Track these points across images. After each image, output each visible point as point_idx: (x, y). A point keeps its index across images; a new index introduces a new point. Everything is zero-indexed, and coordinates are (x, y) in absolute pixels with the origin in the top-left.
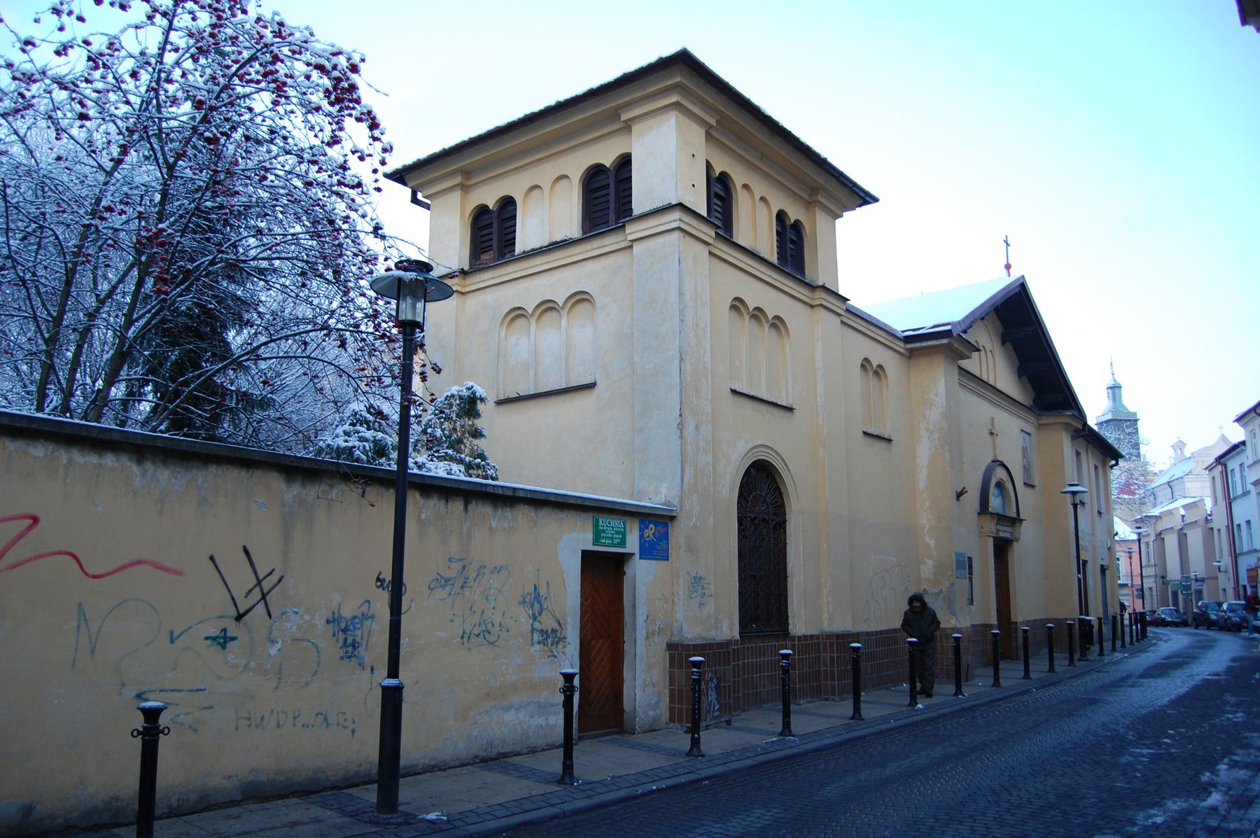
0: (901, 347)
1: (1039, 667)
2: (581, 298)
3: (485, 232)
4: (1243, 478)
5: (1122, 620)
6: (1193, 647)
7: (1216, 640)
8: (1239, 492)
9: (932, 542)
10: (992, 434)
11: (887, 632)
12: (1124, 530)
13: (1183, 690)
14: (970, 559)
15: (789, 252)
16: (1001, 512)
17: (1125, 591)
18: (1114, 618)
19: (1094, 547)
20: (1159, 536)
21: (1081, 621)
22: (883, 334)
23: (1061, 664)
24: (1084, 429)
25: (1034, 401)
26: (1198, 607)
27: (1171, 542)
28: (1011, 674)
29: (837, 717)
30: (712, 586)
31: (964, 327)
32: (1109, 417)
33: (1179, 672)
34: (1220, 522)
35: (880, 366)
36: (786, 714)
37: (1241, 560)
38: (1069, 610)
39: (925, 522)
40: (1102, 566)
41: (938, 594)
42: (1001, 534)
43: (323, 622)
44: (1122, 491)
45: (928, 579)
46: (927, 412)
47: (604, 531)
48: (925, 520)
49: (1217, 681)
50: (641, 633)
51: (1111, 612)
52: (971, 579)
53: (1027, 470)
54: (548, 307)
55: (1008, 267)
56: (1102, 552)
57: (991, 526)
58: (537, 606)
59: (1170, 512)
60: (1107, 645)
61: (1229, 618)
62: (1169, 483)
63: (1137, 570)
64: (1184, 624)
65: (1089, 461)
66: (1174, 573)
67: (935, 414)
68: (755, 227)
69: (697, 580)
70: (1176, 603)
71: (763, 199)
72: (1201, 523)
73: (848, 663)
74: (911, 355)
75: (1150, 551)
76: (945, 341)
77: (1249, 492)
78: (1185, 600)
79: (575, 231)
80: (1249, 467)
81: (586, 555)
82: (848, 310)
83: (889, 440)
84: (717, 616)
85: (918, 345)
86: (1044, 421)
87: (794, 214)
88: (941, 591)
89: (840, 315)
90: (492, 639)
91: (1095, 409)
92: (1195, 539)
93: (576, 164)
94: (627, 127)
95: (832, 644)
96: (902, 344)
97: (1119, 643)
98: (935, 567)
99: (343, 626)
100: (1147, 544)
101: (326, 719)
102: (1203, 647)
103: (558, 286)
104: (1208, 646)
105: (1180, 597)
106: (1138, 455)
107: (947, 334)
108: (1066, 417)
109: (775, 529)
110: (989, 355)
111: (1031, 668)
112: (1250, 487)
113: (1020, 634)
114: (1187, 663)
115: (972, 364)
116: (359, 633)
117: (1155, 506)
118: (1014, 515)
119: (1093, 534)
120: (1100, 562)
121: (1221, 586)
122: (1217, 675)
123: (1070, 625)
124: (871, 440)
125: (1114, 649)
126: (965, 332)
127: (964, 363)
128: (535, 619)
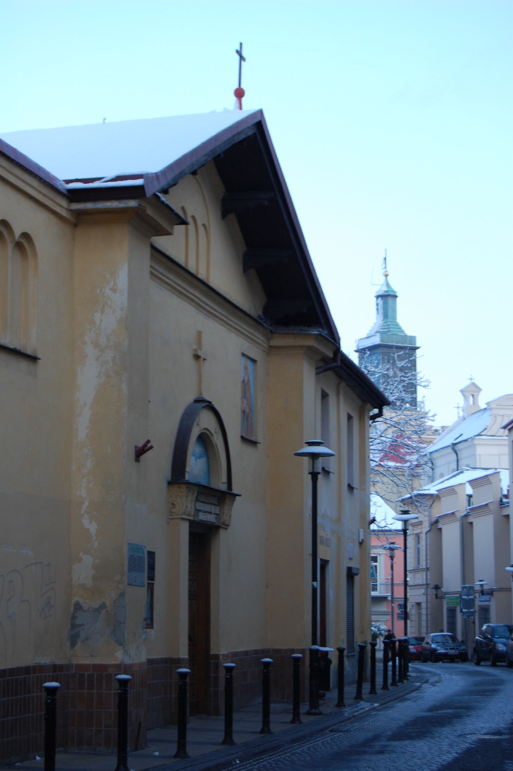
0: (62, 206)
1: (247, 725)
5: (373, 651)
6: (471, 693)
7: (502, 682)
9: (92, 527)
10: (197, 357)
11: (12, 671)
12: (384, 514)
13: (448, 758)
14: (151, 555)
16: (204, 482)
17: (383, 608)
18: (362, 648)
19: (339, 539)
20: (435, 525)
21: (314, 653)
22: (35, 183)
23: (281, 721)
24: (334, 359)
26: (482, 633)
27: (451, 534)
28: (205, 736)
31: (163, 183)
32: (376, 340)
33: (446, 731)
35: (26, 236)
38: (297, 637)
39: (83, 493)
40: (349, 569)
42: (202, 517)
44: (386, 456)
46: (97, 316)
48: (84, 490)
49: (498, 741)
51: (358, 640)
52: (151, 588)
53: (247, 416)
55: (239, 93)
56: (351, 548)
57: (186, 503)
59: (451, 490)
60: (350, 690)
62: (454, 445)
63: (399, 579)
64: (462, 657)
65: (340, 408)
66: (452, 582)
67: (109, 321)
70: (452, 627)
74: (78, 221)
75: (417, 551)
76: (132, 203)
78: (465, 623)
83: (33, 359)
85: (90, 206)
86: (277, 341)
88: (103, 606)
91: (354, 328)
92: (484, 529)
96: (64, 203)
97: (366, 687)
100: (418, 536)
102: (483, 693)
104: (488, 690)
105: (459, 618)
106: (414, 402)
107: (136, 192)
110: (201, 230)
111: (236, 727)
113: (222, 675)
115: (173, 244)
117: (432, 479)
118: (223, 487)
119: (339, 520)
120: (346, 563)
122: (498, 733)
123: (297, 659)
125: (359, 696)
126: (165, 191)
127: (161, 242)
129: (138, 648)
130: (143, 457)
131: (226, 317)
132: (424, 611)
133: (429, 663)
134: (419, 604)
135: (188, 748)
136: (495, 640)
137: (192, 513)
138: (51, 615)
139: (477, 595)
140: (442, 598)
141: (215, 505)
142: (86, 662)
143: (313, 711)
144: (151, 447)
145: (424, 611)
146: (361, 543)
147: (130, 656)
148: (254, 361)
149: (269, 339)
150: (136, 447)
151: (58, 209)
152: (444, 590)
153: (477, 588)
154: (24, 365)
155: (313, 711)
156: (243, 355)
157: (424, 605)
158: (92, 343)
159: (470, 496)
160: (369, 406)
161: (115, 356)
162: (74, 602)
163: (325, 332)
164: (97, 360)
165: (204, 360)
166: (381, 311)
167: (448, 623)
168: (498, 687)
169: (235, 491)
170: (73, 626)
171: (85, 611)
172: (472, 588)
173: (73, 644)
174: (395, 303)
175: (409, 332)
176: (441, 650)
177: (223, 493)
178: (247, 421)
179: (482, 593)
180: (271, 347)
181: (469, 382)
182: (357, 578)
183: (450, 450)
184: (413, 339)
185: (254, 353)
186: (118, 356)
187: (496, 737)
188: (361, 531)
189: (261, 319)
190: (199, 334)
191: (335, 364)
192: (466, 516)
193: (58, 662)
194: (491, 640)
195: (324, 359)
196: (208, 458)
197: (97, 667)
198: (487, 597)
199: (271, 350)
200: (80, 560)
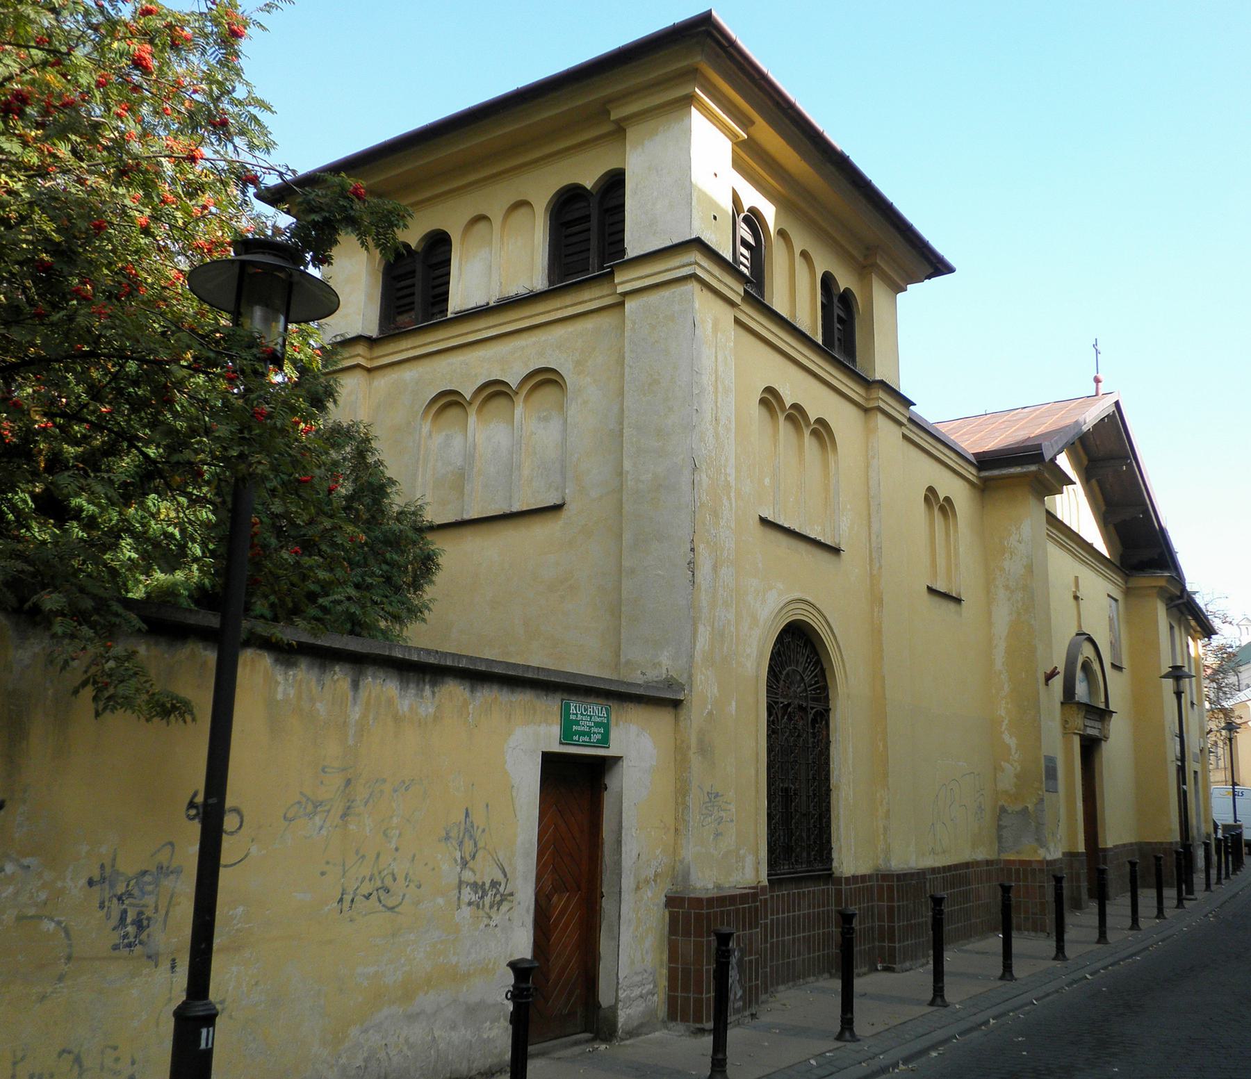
2: (545, 379)
3: (403, 284)
10: (1076, 598)
15: (837, 335)
30: (733, 807)
42: (1090, 732)
43: (83, 881)
47: (577, 723)
50: (627, 882)
53: (1114, 646)
54: (495, 391)
55: (1097, 380)
57: (1078, 721)
58: (469, 846)
68: (795, 294)
69: (714, 796)
71: (804, 254)
73: (924, 912)
76: (1033, 468)
79: (539, 282)
81: (549, 760)
82: (911, 420)
83: (958, 601)
84: (733, 855)
87: (844, 281)
89: (900, 424)
90: (391, 902)
93: (541, 189)
94: (619, 132)
95: (890, 888)
98: (1017, 776)
99: (121, 889)
101: (78, 1060)
103: (510, 360)
108: (1160, 579)
109: (814, 721)
116: (150, 900)
118: (1102, 706)
124: (936, 599)
128: (465, 864)
148: (1116, 600)
151: (970, 477)
154: (952, 606)
169: (1111, 708)
190: (1077, 578)
193: (989, 858)
197: (1022, 862)
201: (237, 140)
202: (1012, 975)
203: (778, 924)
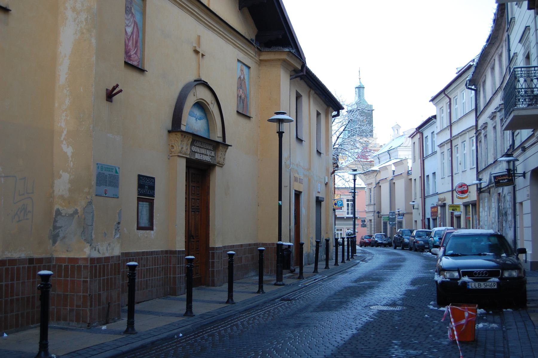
4: (433, 142)
7: (404, 260)
8: (430, 152)
9: (69, 151)
10: (197, 52)
16: (205, 135)
19: (309, 180)
21: (278, 245)
24: (302, 70)
25: (257, 36)
27: (385, 188)
29: (172, 315)
34: (416, 175)
36: (189, 300)
37: (427, 200)
39: (63, 124)
41: (72, 215)
42: (197, 156)
45: (62, 196)
53: (242, 100)
57: (183, 146)
59: (385, 168)
60: (308, 269)
61: (417, 242)
64: (389, 245)
66: (385, 210)
72: (405, 175)
77: (436, 152)
78: (391, 228)
80: (438, 134)
86: (265, 56)
88: (76, 212)
92: (400, 185)
98: (71, 182)
104: (394, 266)
105: (389, 227)
108: (283, 55)
112: (437, 149)
114: (371, 287)
118: (220, 140)
119: (309, 169)
121: (414, 219)
122: (394, 304)
129: (109, 244)
130: (115, 98)
131: (223, 32)
132: (373, 224)
133: (369, 247)
134: (371, 220)
135: (329, 266)
136: (403, 237)
137: (188, 153)
138: (27, 219)
139: (397, 216)
140: (381, 217)
141: (210, 150)
142: (64, 256)
143: (279, 283)
144: (121, 91)
145: (373, 224)
146: (326, 184)
147: (99, 251)
148: (249, 68)
149: (259, 55)
150: (107, 90)
152: (382, 214)
153: (397, 213)
155: (279, 283)
156: (238, 61)
157: (373, 221)
158: (71, 8)
159: (394, 171)
160: (331, 109)
161: (87, 17)
162: (55, 209)
163: (293, 51)
164: (75, 21)
165: (203, 55)
166: (357, 94)
167: (384, 229)
168: (402, 264)
169: (227, 142)
170: (55, 228)
171: (63, 216)
172: (394, 212)
173: (54, 242)
174: (363, 90)
175: (369, 103)
176: (380, 241)
177: (218, 143)
178: (243, 103)
179: (399, 215)
180: (260, 60)
181: (396, 124)
182: (323, 204)
183: (387, 153)
184: (371, 106)
185: (247, 61)
186: (89, 17)
187: (392, 309)
188: (326, 177)
189: (253, 41)
191: (302, 73)
192: (392, 179)
194: (401, 237)
195: (295, 71)
196: (208, 121)
197: (71, 260)
198: (401, 217)
199: (261, 62)
200: (60, 177)
201: (367, 154)
202: (263, 291)
203: (155, 259)
